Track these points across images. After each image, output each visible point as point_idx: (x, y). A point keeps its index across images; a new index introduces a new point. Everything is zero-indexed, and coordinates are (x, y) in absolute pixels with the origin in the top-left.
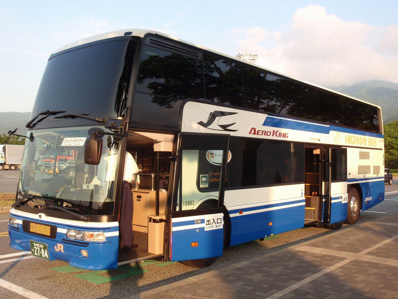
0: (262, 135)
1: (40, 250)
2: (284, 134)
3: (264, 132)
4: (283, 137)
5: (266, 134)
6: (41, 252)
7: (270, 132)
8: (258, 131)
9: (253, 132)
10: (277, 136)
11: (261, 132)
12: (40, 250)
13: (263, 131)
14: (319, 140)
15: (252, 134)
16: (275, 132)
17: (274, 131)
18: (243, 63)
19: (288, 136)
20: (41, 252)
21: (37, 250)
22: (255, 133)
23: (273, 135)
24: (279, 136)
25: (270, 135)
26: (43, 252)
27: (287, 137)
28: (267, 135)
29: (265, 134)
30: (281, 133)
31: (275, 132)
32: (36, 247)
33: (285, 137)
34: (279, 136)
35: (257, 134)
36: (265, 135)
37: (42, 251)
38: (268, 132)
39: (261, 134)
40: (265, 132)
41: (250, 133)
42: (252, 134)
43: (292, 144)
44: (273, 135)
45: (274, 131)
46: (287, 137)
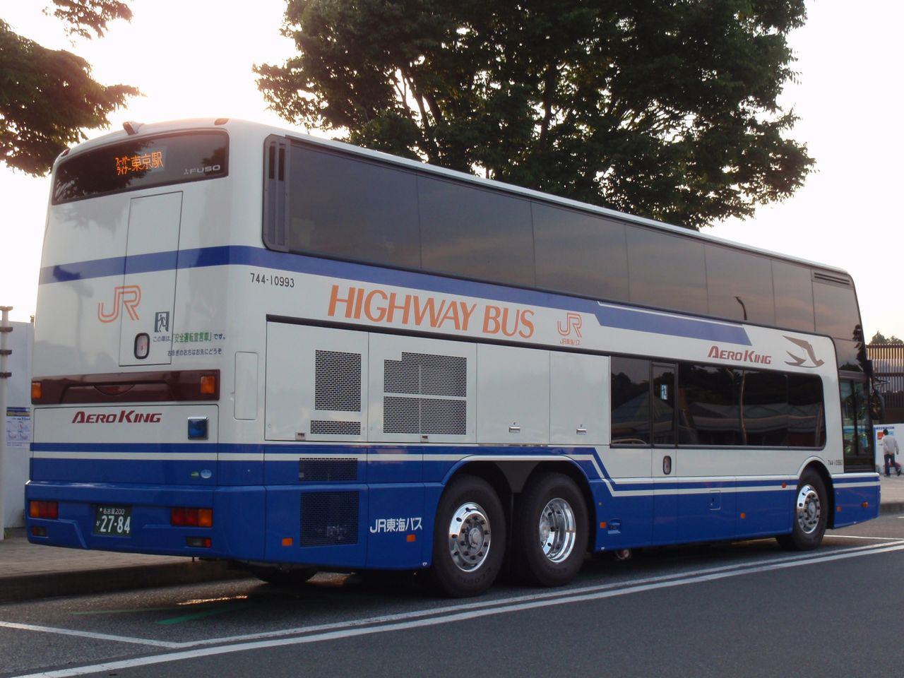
0: (97, 421)
1: (116, 520)
2: (763, 356)
3: (731, 354)
4: (762, 362)
5: (105, 420)
6: (116, 524)
7: (741, 354)
8: (89, 417)
9: (714, 354)
10: (751, 361)
11: (727, 354)
12: (116, 520)
13: (730, 352)
14: (772, 208)
15: (78, 422)
16: (749, 354)
17: (747, 352)
18: (395, 329)
19: (770, 361)
20: (116, 524)
21: (109, 520)
22: (716, 356)
23: (745, 360)
24: (755, 361)
25: (740, 359)
26: (120, 524)
27: (769, 363)
28: (736, 359)
29: (732, 356)
30: (759, 356)
31: (749, 354)
32: (107, 515)
33: (766, 363)
34: (755, 361)
35: (721, 357)
36: (103, 421)
37: (119, 521)
38: (737, 353)
39: (94, 420)
40: (733, 353)
41: (710, 356)
42: (78, 422)
43: (83, 544)
44: (745, 360)
45: (747, 352)
46: (769, 363)
